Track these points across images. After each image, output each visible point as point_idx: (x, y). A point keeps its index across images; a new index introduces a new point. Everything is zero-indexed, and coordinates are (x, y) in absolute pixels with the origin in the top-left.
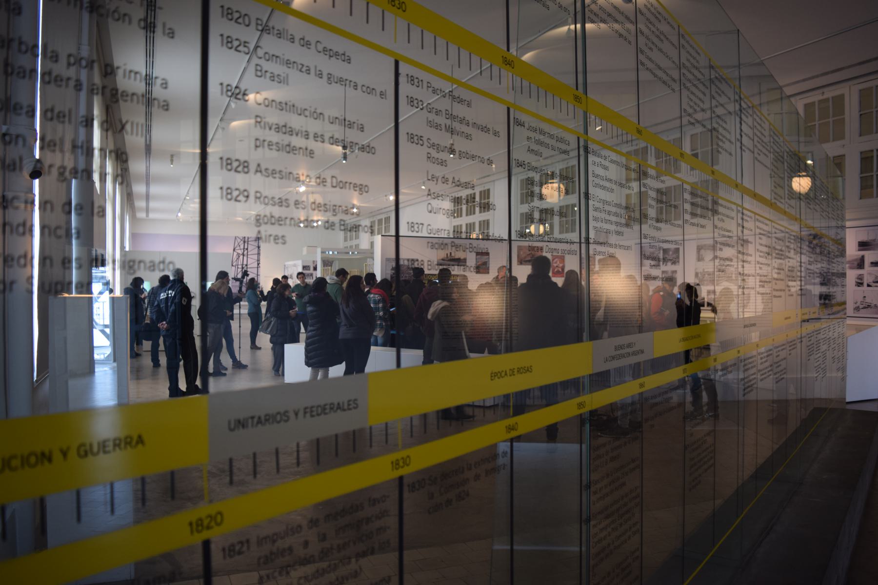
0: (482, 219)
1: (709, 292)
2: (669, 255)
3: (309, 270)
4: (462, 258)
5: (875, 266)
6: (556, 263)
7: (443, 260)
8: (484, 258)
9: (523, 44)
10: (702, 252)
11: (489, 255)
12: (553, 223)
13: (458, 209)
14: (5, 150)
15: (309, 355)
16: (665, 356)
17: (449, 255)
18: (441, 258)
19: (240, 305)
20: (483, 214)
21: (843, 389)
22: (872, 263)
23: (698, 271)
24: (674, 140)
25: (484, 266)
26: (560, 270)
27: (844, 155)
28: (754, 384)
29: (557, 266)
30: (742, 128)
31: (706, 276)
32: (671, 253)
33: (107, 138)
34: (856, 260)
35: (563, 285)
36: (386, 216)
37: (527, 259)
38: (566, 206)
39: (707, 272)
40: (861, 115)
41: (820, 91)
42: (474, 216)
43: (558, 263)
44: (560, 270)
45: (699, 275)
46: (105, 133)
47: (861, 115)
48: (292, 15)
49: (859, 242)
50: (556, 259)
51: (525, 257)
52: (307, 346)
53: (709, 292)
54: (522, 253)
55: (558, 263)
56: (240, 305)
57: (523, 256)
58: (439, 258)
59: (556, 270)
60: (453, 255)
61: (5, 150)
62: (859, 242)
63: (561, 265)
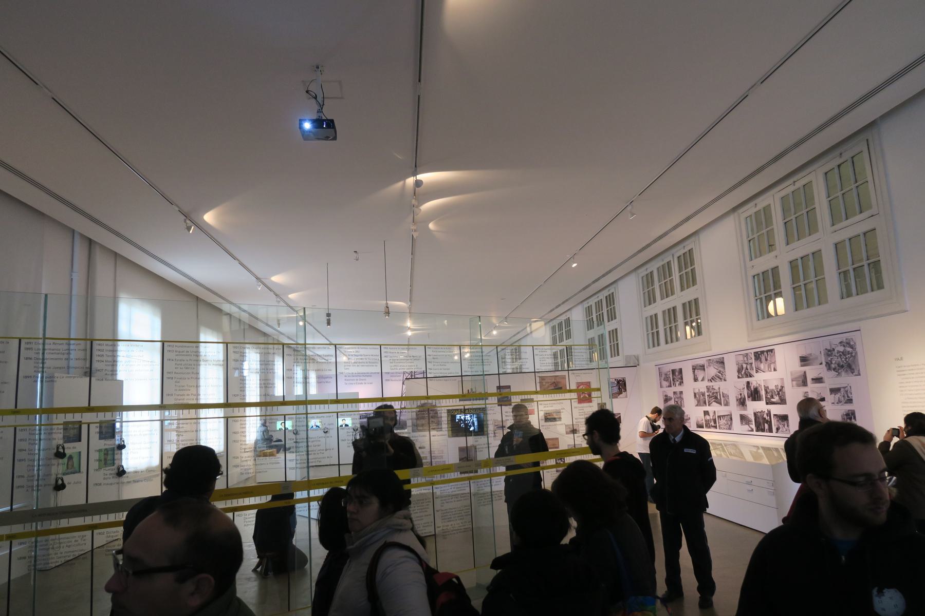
0: (666, 307)
2: (676, 376)
5: (816, 383)
11: (510, 388)
12: (658, 331)
13: (611, 309)
20: (686, 291)
21: (198, 439)
22: (813, 379)
23: (697, 391)
24: (764, 208)
27: (777, 267)
34: (799, 377)
36: (596, 300)
38: (689, 302)
40: (785, 223)
41: (837, 152)
42: (696, 287)
47: (785, 223)
48: (294, 401)
49: (800, 357)
52: (753, 463)
59: (582, 396)
62: (800, 357)
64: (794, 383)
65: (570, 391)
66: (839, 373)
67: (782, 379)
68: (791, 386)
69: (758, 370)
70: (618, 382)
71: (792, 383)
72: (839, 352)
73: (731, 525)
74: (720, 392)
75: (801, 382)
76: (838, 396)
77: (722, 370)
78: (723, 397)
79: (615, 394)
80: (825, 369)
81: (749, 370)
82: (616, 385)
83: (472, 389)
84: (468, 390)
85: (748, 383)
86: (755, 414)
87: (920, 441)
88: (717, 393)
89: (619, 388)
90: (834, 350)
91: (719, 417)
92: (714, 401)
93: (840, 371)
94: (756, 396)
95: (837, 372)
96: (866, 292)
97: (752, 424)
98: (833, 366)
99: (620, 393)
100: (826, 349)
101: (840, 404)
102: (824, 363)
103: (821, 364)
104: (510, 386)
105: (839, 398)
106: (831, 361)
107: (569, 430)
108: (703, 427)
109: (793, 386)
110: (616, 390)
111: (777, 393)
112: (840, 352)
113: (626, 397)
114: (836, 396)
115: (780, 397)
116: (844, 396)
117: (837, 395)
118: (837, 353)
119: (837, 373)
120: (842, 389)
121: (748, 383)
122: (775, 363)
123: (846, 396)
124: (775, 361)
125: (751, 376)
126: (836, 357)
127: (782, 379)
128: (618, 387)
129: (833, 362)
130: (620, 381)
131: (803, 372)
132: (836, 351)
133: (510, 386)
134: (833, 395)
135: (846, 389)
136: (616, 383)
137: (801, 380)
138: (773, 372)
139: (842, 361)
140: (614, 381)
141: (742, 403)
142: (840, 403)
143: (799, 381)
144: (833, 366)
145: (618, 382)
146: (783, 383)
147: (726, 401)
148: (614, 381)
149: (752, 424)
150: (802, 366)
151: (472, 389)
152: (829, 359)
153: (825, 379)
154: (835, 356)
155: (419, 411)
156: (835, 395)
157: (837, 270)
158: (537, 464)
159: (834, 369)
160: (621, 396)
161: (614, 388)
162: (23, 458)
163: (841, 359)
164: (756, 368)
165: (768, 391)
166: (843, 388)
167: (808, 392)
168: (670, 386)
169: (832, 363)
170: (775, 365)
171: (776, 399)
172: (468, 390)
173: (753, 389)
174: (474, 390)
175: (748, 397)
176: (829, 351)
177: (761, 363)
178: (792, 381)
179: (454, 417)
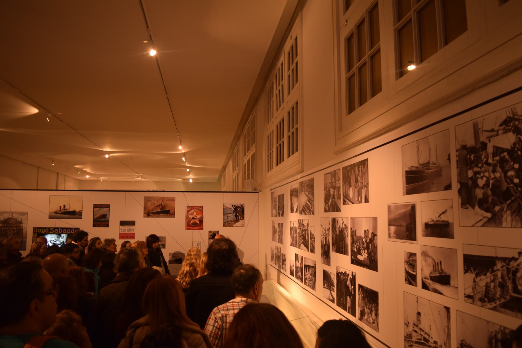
4: (77, 211)
7: (55, 213)
8: (103, 211)
9: (305, 314)
14: (452, 286)
15: (343, 253)
17: (62, 208)
25: (103, 219)
26: (198, 222)
28: (372, 315)
29: (193, 218)
30: (489, 129)
37: (156, 211)
43: (195, 214)
44: (198, 222)
46: (150, 216)
50: (192, 211)
51: (154, 209)
55: (195, 214)
57: (151, 208)
58: (50, 211)
61: (452, 286)
63: (199, 217)
64: (393, 228)
66: (494, 215)
67: (375, 219)
68: (387, 236)
69: (346, 199)
71: (389, 230)
72: (498, 151)
74: (308, 230)
75: (404, 229)
76: (484, 280)
77: (311, 196)
78: (310, 239)
79: (230, 221)
80: (457, 201)
81: (336, 199)
82: (233, 212)
83: (64, 206)
84: (61, 207)
85: (334, 220)
86: (338, 274)
88: (305, 230)
89: (236, 216)
90: (484, 146)
91: (306, 266)
92: (356, 235)
93: (497, 208)
94: (341, 243)
95: (487, 211)
97: (334, 291)
98: (479, 193)
99: (237, 221)
100: (464, 147)
101: (489, 306)
102: (455, 186)
103: (448, 187)
104: (109, 205)
105: (487, 286)
106: (474, 179)
109: (390, 237)
110: (232, 217)
111: (365, 245)
112: (503, 150)
113: (243, 225)
114: (478, 280)
115: (369, 254)
116: (502, 286)
117: (483, 277)
118: (494, 155)
119: (489, 215)
120: (499, 265)
121: (334, 220)
122: (367, 186)
123: (510, 286)
124: (368, 184)
125: (338, 210)
126: (491, 168)
127: (375, 219)
128: (235, 214)
129: (481, 182)
130: (238, 207)
131: (410, 208)
132: (490, 149)
133: (109, 205)
134: (471, 276)
135: (514, 264)
136: (233, 209)
137: (404, 224)
138: (364, 205)
139: (505, 176)
140: (230, 206)
141: (326, 254)
142: (490, 301)
143: (401, 226)
144: (479, 193)
146: (375, 227)
147: (313, 245)
148: (230, 206)
149: (334, 291)
150: (409, 192)
151: (64, 206)
152: (470, 174)
153: (457, 230)
154: (487, 163)
156: (477, 275)
157: (473, 303)
159: (483, 204)
160: (237, 224)
161: (230, 215)
163: (505, 172)
164: (343, 195)
165: (355, 238)
166: (504, 259)
167: (415, 255)
169: (476, 185)
170: (367, 191)
171: (363, 257)
172: (61, 207)
173: (338, 233)
174: (67, 207)
175: (333, 245)
176: (472, 150)
177: (350, 186)
178: (390, 225)
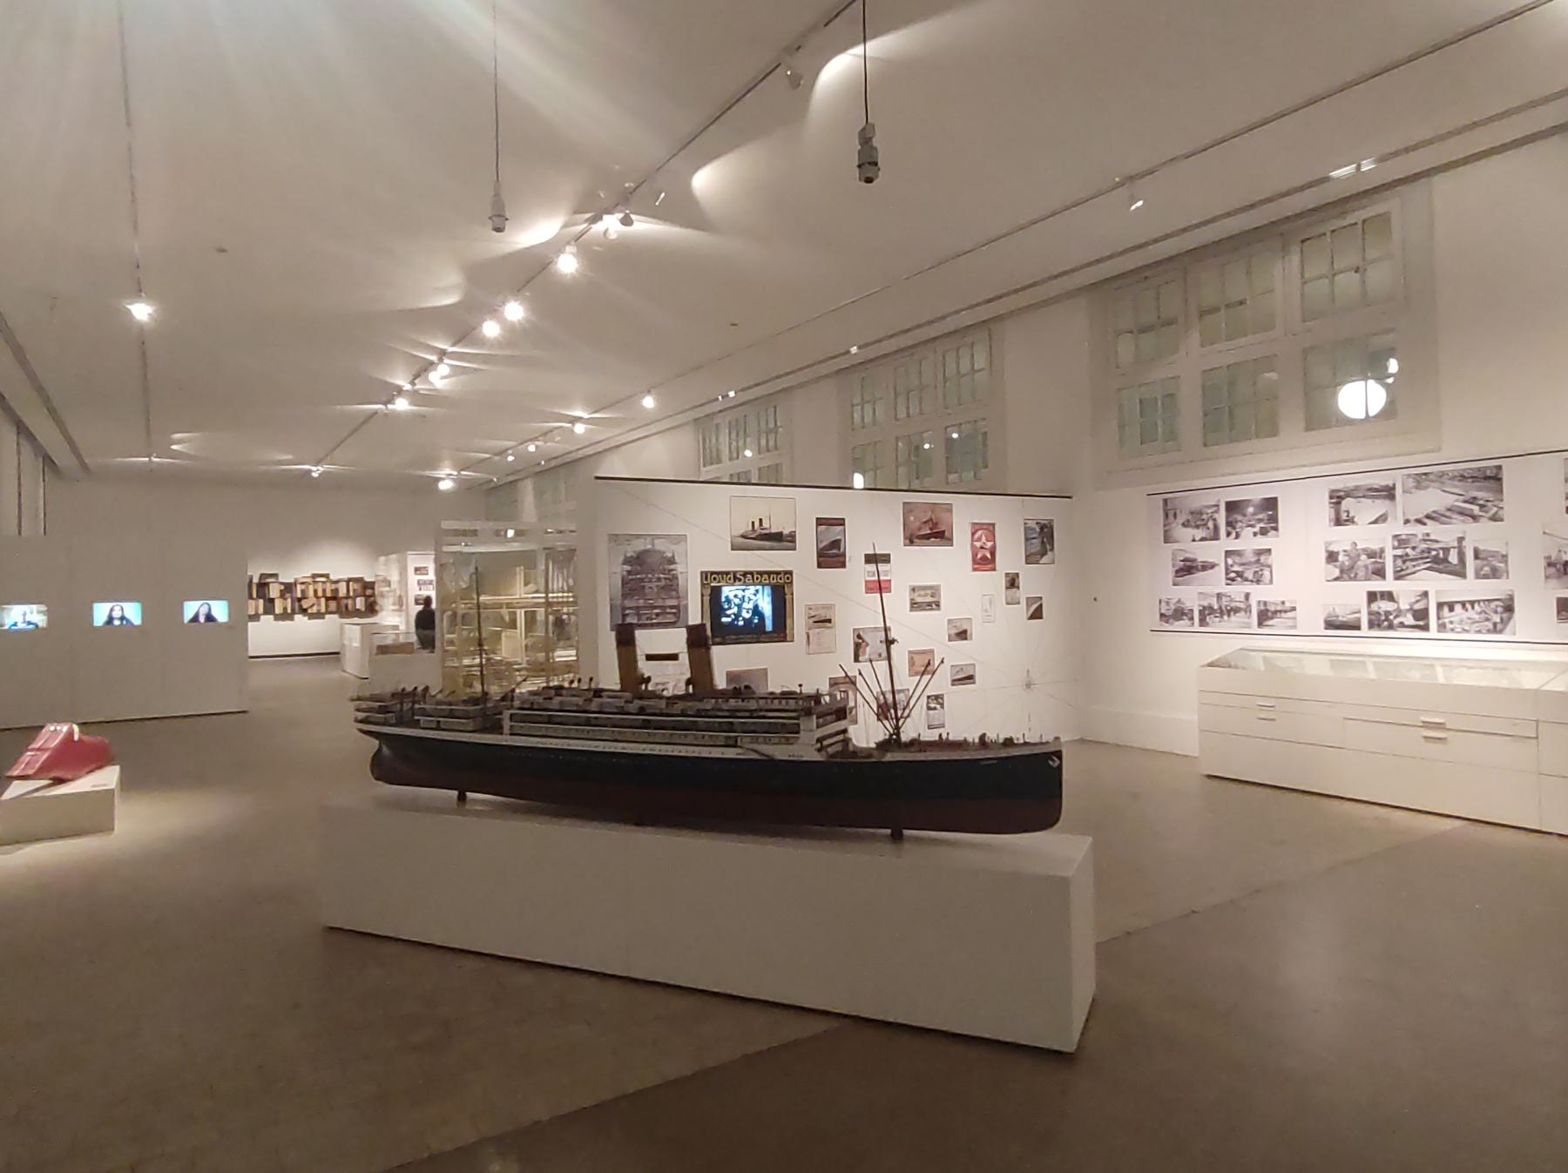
1: (748, 612)
3: (427, 574)
6: (979, 539)
7: (743, 536)
10: (1347, 504)
11: (843, 524)
16: (640, 822)
17: (757, 524)
18: (741, 532)
19: (590, 684)
26: (989, 556)
29: (982, 548)
31: (1364, 557)
32: (1251, 510)
33: (1309, 239)
35: (230, 615)
39: (1364, 550)
43: (984, 539)
45: (1341, 558)
50: (979, 533)
53: (748, 612)
54: (912, 518)
56: (590, 684)
59: (979, 556)
60: (766, 524)
63: (989, 544)
65: (623, 602)
70: (1042, 527)
73: (1521, 835)
79: (1035, 554)
87: (850, 55)
96: (1384, 563)
99: (1043, 554)
107: (954, 631)
108: (1358, 628)
128: (1040, 540)
136: (1038, 530)
145: (1042, 527)
155: (629, 573)
158: (845, 731)
160: (1044, 560)
161: (1034, 541)
162: (786, 532)
168: (1216, 537)
179: (716, 592)
